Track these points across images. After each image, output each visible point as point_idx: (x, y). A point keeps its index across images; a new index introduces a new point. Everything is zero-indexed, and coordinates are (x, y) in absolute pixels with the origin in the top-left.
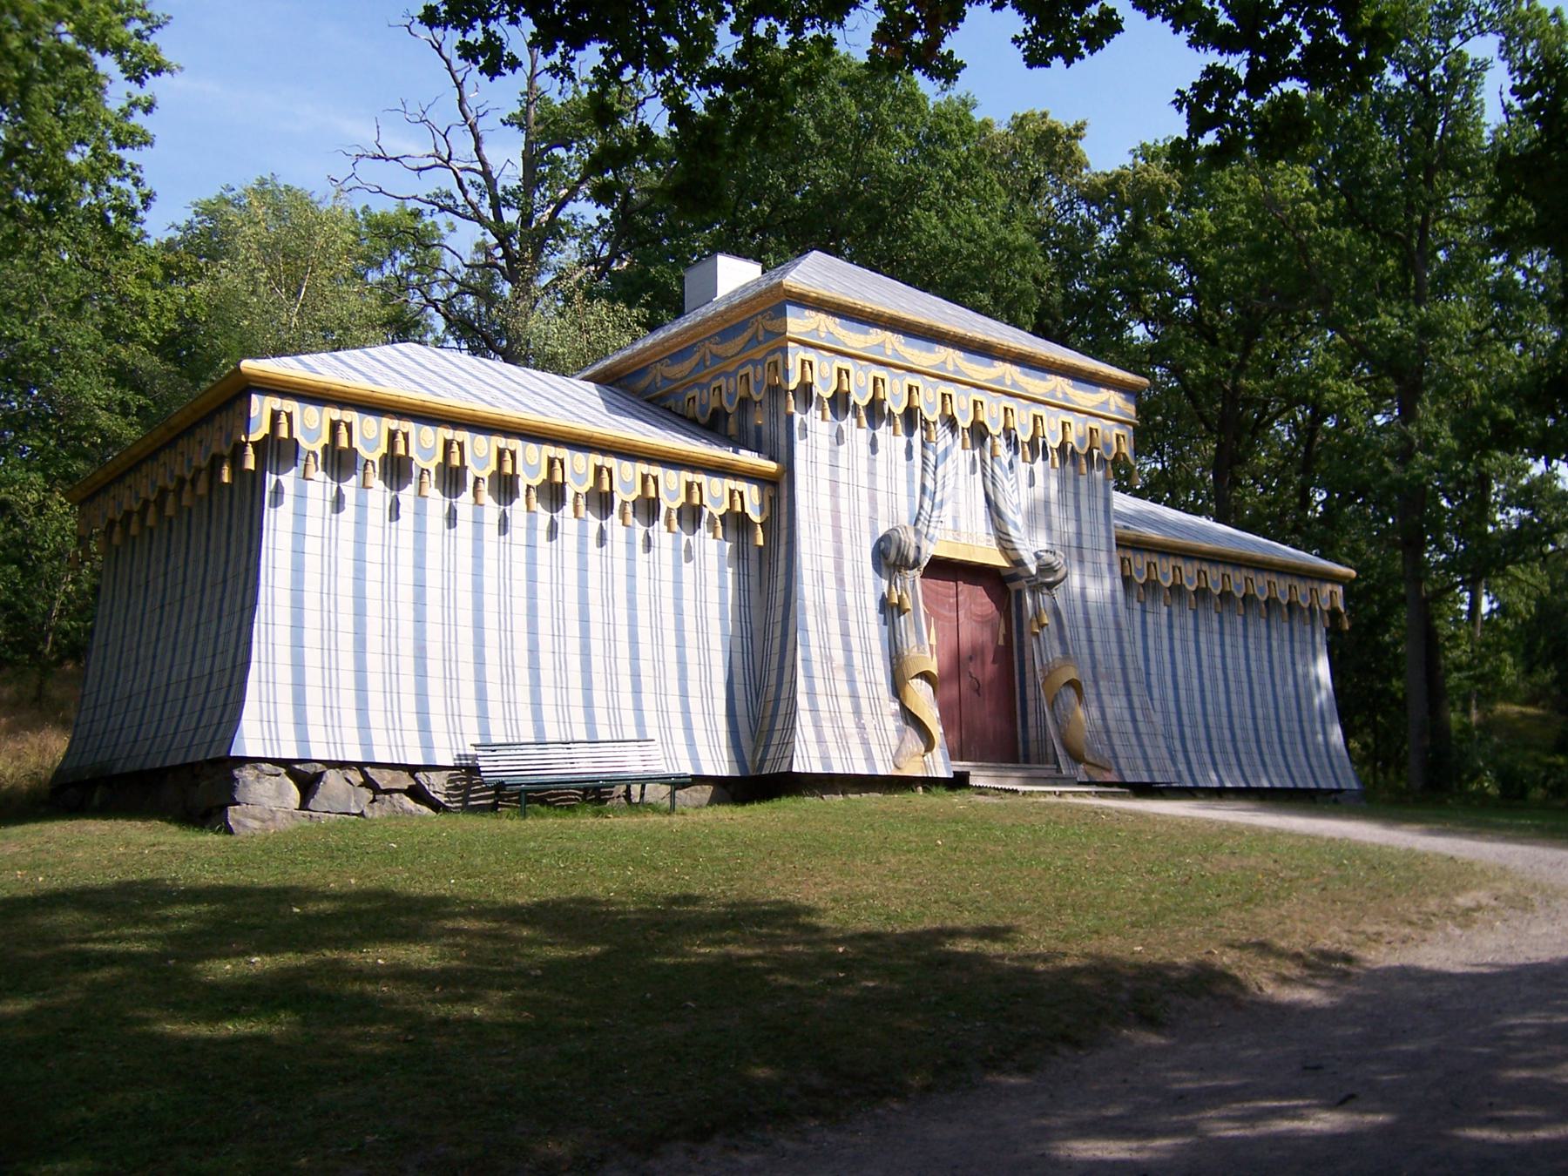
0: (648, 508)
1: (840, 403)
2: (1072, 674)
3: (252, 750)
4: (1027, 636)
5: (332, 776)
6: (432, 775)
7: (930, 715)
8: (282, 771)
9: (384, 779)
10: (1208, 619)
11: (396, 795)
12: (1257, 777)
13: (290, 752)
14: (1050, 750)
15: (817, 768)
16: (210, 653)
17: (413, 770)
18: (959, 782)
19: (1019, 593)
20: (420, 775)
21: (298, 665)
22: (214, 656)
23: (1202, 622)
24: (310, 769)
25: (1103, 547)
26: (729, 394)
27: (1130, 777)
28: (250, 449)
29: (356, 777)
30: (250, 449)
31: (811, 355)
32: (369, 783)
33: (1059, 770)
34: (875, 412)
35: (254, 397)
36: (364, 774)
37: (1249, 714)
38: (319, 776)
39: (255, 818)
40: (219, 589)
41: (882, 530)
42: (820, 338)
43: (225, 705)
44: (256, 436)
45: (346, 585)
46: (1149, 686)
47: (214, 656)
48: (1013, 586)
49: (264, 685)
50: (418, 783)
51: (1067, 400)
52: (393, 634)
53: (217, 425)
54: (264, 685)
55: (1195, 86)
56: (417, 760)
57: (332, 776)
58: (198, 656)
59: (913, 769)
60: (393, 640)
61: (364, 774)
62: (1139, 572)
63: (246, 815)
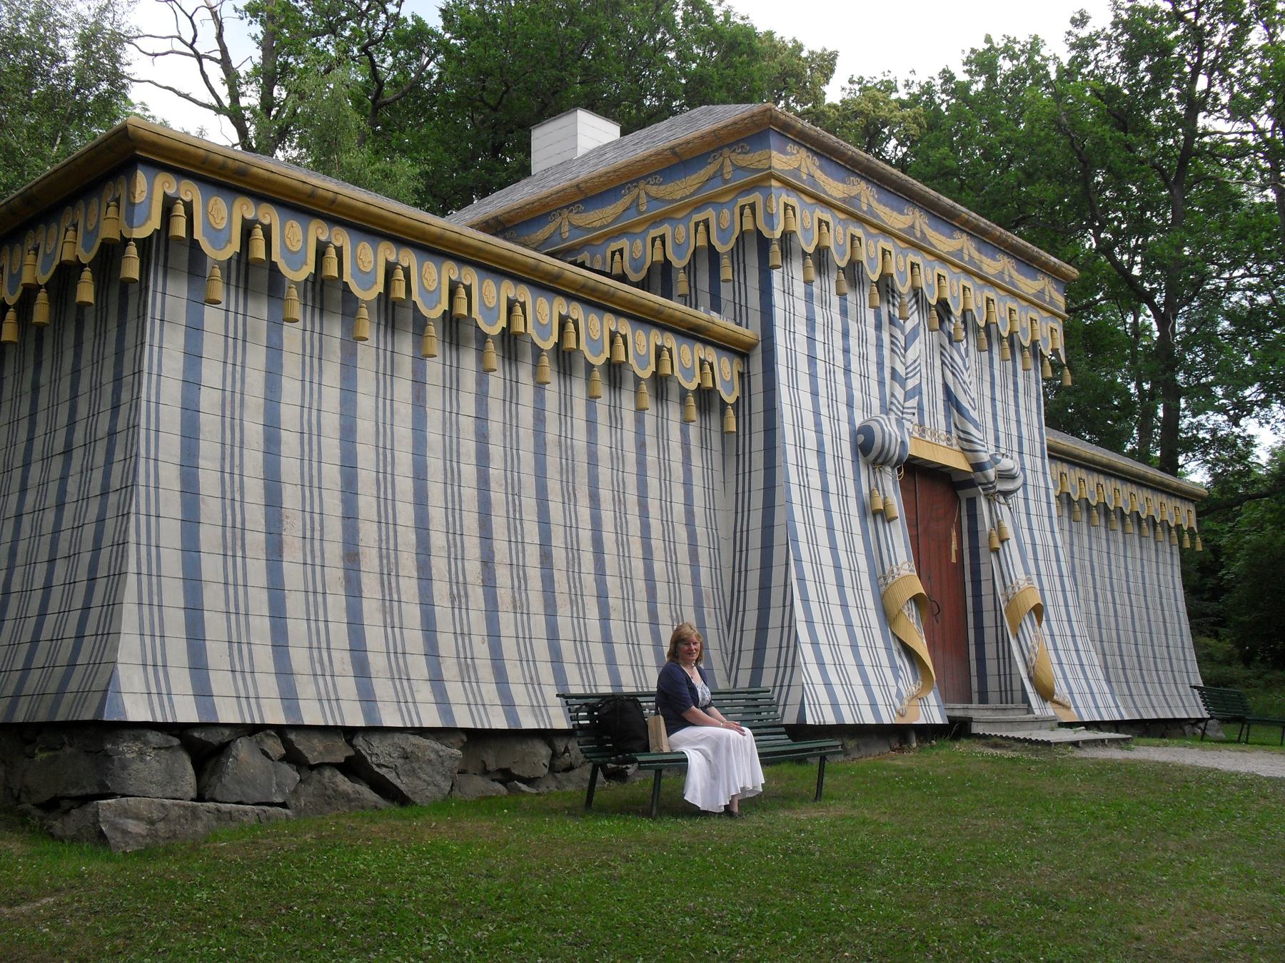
1: (821, 258)
3: (136, 711)
4: (983, 551)
6: (375, 740)
7: (921, 646)
8: (176, 742)
9: (314, 750)
11: (327, 773)
12: (1180, 712)
13: (187, 712)
14: (1017, 686)
16: (44, 556)
17: (349, 733)
18: (957, 729)
19: (972, 503)
21: (192, 581)
22: (52, 561)
24: (215, 738)
25: (1038, 453)
26: (721, 230)
28: (132, 250)
29: (276, 748)
30: (132, 250)
31: (793, 200)
32: (293, 757)
33: (1029, 710)
34: (853, 273)
35: (141, 177)
36: (287, 744)
37: (1115, 640)
38: (223, 749)
39: (137, 817)
40: (57, 463)
41: (859, 421)
42: (800, 179)
43: (80, 637)
44: (142, 232)
45: (254, 460)
47: (52, 561)
48: (964, 494)
49: (146, 609)
50: (358, 752)
51: (1013, 284)
52: (317, 535)
53: (30, 244)
54: (146, 609)
55: (812, 53)
57: (243, 749)
58: (20, 559)
60: (317, 544)
61: (287, 744)
63: (125, 813)
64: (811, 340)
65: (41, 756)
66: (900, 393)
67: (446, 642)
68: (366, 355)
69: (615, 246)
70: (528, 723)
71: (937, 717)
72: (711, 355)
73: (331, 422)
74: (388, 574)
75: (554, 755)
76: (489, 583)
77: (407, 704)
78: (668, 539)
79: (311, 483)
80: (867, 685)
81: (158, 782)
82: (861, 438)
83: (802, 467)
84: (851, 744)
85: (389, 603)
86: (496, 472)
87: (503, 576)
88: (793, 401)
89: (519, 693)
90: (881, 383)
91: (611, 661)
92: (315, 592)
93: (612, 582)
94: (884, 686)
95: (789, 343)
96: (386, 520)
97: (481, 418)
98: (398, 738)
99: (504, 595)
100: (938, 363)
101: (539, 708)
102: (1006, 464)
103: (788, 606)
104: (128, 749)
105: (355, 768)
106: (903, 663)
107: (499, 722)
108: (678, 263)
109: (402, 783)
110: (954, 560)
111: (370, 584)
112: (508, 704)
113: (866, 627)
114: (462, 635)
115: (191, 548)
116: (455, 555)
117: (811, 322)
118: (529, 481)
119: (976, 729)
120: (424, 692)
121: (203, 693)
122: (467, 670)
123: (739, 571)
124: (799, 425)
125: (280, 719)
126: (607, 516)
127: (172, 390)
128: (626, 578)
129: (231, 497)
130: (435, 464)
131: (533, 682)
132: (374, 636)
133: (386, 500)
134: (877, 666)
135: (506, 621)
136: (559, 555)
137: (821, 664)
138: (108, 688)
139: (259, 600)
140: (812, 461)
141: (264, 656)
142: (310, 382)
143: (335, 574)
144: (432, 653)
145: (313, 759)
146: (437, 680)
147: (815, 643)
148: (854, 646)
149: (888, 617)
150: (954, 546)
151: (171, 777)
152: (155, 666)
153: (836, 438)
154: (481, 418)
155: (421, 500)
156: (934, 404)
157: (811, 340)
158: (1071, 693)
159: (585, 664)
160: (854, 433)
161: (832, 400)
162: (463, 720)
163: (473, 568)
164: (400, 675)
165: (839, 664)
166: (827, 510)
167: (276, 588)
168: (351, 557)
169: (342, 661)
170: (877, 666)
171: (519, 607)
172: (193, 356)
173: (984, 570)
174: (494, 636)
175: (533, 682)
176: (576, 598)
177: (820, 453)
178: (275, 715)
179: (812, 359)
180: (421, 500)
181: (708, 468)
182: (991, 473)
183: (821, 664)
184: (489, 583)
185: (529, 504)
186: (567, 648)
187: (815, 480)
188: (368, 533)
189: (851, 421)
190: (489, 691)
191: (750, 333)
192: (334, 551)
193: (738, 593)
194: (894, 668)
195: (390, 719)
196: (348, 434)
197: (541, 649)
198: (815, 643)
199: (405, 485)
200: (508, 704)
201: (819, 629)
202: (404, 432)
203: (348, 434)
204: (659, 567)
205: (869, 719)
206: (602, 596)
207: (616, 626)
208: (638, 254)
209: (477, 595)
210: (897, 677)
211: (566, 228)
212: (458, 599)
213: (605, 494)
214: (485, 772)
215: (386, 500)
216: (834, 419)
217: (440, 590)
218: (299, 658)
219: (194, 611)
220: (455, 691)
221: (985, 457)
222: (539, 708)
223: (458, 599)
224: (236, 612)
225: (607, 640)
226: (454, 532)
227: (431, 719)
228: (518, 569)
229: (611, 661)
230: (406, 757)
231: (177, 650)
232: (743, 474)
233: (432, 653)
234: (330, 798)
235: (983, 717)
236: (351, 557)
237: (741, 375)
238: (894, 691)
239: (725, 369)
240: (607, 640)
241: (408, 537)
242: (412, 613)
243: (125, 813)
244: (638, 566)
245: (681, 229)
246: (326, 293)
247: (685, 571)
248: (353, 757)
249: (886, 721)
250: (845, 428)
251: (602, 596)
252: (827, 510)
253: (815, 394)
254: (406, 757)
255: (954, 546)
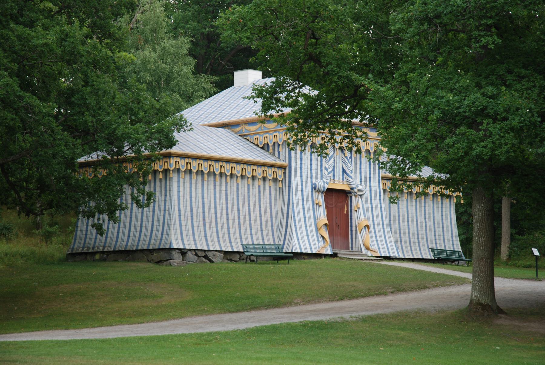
0: (200, 172)
2: (366, 223)
3: (175, 247)
4: (353, 211)
5: (189, 253)
7: (327, 236)
9: (200, 254)
10: (412, 201)
13: (182, 247)
14: (359, 246)
15: (299, 251)
17: (205, 251)
18: (334, 255)
19: (351, 197)
20: (206, 252)
23: (409, 202)
24: (185, 251)
27: (383, 255)
29: (194, 253)
36: (196, 252)
38: (186, 253)
46: (390, 225)
48: (349, 195)
56: (206, 249)
57: (189, 253)
59: (324, 252)
61: (196, 252)
62: (183, 166)
64: (301, 164)
65: (155, 254)
66: (326, 173)
67: (220, 235)
68: (206, 183)
69: (256, 137)
70: (235, 250)
71: (329, 252)
72: (276, 170)
73: (200, 195)
74: (210, 223)
75: (240, 257)
76: (228, 224)
77: (214, 246)
78: (266, 212)
79: (197, 207)
80: (310, 244)
81: (177, 256)
82: (314, 186)
83: (297, 195)
84: (306, 257)
85: (210, 228)
86: (229, 201)
87: (230, 221)
88: (296, 179)
89: (234, 244)
90: (321, 171)
91: (252, 238)
92: (198, 226)
93: (253, 222)
94: (315, 245)
95: (295, 166)
96: (210, 213)
97: (226, 191)
98: (213, 252)
99: (231, 226)
100: (341, 161)
101: (237, 247)
102: (360, 187)
103: (291, 227)
104: (174, 252)
105: (206, 257)
106: (321, 239)
107: (230, 250)
108: (271, 145)
109: (213, 260)
110: (345, 213)
111: (207, 225)
112: (232, 247)
113: (312, 231)
114: (223, 233)
115: (180, 220)
116: (222, 218)
117: (301, 159)
118: (236, 202)
119: (339, 255)
120: (217, 244)
121: (183, 244)
122: (224, 240)
123: (282, 218)
124: (296, 185)
125: (195, 248)
126: (252, 208)
127: (176, 193)
128: (256, 221)
129: (185, 211)
130: (218, 201)
131: (236, 242)
132: (208, 234)
133: (209, 209)
134: (313, 240)
135: (231, 231)
136: (241, 217)
137: (298, 239)
138: (171, 243)
139: (190, 228)
140: (300, 193)
141: (191, 237)
142: (197, 188)
143: (202, 223)
144: (218, 237)
145: (199, 255)
146: (219, 242)
147: (297, 235)
148: (308, 236)
149: (317, 229)
150: (346, 209)
151: (179, 257)
152: (176, 239)
153: (307, 187)
154: (226, 191)
155: (215, 208)
156: (339, 173)
157: (301, 164)
158: (379, 248)
159: (247, 239)
160: (312, 185)
161: (306, 177)
162: (224, 249)
163: (225, 221)
164: (213, 241)
165: (303, 240)
166: (303, 204)
167: (193, 226)
168: (204, 220)
169: (203, 238)
170: (313, 240)
171: (234, 228)
172: (179, 187)
173: (353, 215)
174: (229, 233)
175: (236, 242)
176: (245, 226)
177: (302, 191)
178: (194, 248)
179: (301, 168)
180: (215, 208)
181: (275, 195)
182: (356, 190)
183: (298, 239)
184: (228, 224)
185: (236, 207)
186: (243, 236)
187: (300, 197)
188: (207, 215)
189: (311, 182)
190: (228, 244)
191: (286, 163)
192: (201, 219)
193: (282, 223)
194: (318, 241)
195: (212, 249)
196: (203, 197)
197: (238, 236)
198: (297, 235)
199: (213, 206)
200: (232, 247)
201: (299, 232)
202: (212, 196)
203: (203, 197)
204: (263, 218)
205: (309, 252)
206: (250, 225)
207: (253, 231)
208: (261, 140)
209: (226, 226)
210: (319, 243)
211: (244, 129)
212: (222, 227)
213: (251, 203)
214: (227, 259)
215: (209, 209)
216: (307, 182)
217: (219, 225)
218: (197, 238)
219: (181, 230)
220: (222, 244)
221: (353, 186)
222: (237, 247)
223: (222, 227)
224: (187, 230)
225: (251, 234)
226: (222, 214)
227: (218, 249)
228: (233, 220)
229: (252, 238)
230: (214, 255)
231: (179, 236)
232: (284, 196)
233: (218, 237)
234: (203, 262)
235: (342, 253)
236: (204, 220)
237: (284, 173)
238: (317, 246)
239: (280, 172)
240: (251, 234)
241: (213, 215)
242: (214, 229)
243: (174, 262)
244: (258, 218)
245: (271, 136)
246: (200, 172)
247: (269, 219)
248: (204, 255)
249: (314, 252)
250: (310, 184)
251: (250, 225)
252: (303, 204)
253: (301, 176)
254: (214, 255)
255: (346, 209)
